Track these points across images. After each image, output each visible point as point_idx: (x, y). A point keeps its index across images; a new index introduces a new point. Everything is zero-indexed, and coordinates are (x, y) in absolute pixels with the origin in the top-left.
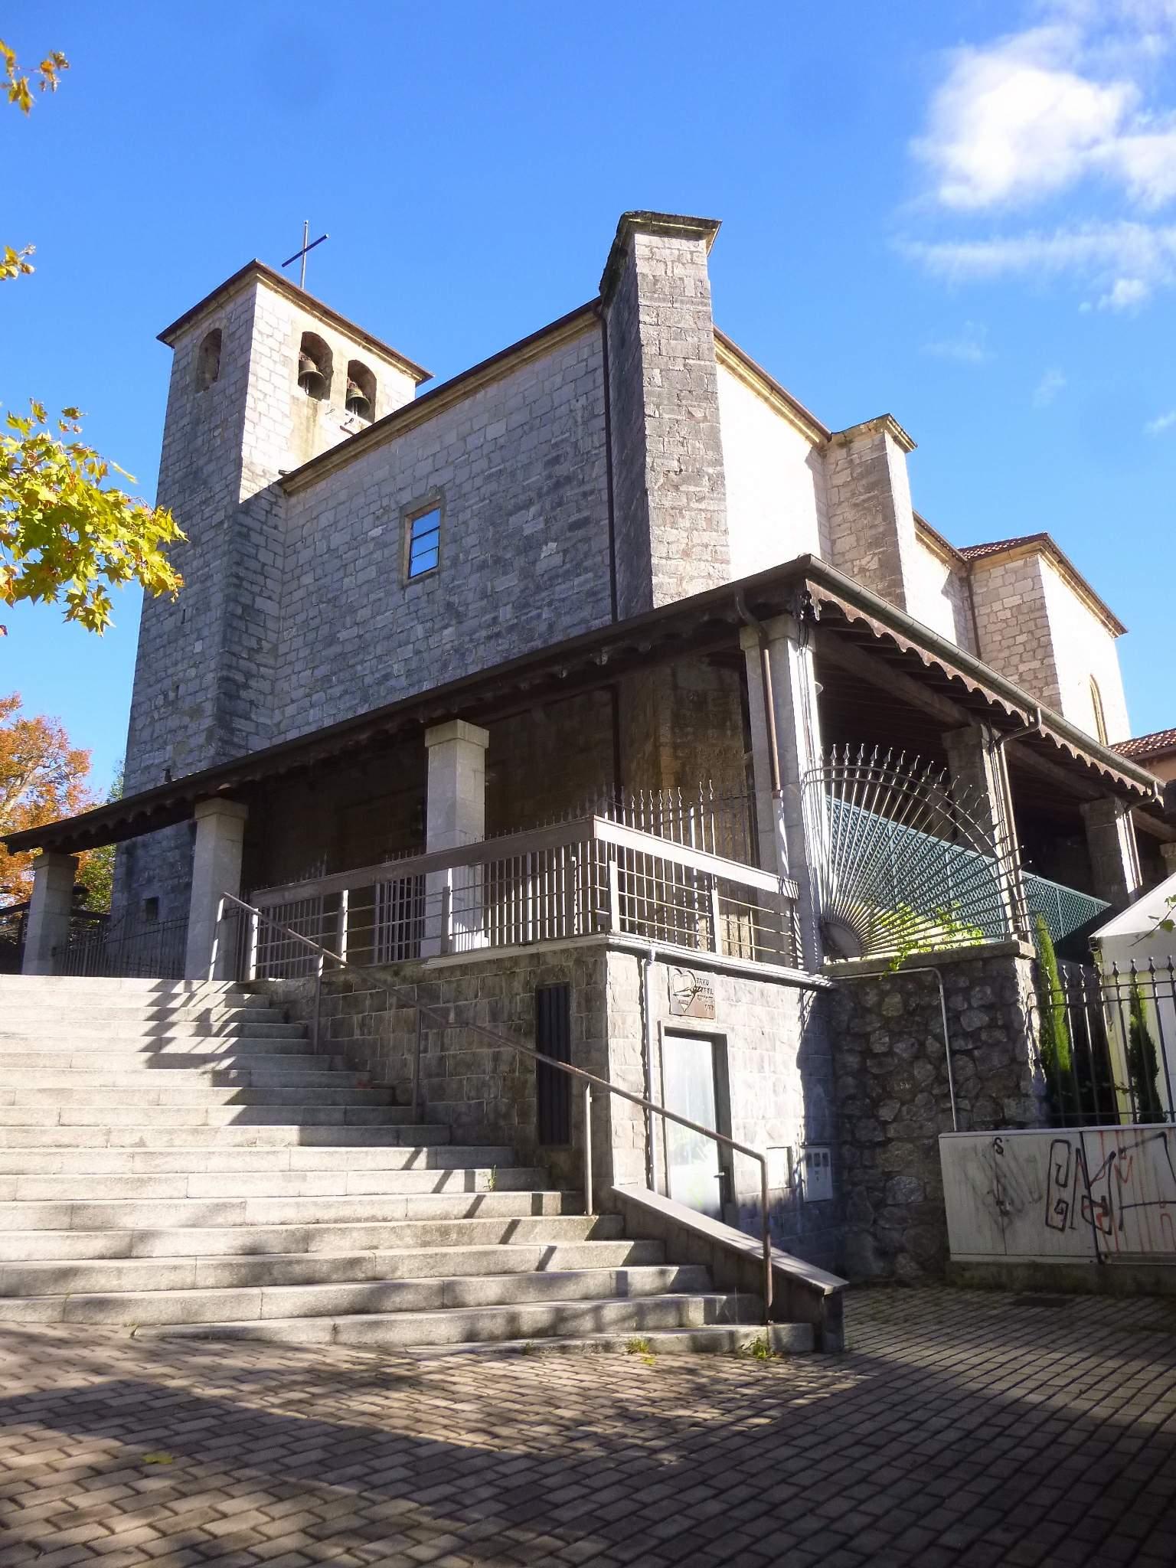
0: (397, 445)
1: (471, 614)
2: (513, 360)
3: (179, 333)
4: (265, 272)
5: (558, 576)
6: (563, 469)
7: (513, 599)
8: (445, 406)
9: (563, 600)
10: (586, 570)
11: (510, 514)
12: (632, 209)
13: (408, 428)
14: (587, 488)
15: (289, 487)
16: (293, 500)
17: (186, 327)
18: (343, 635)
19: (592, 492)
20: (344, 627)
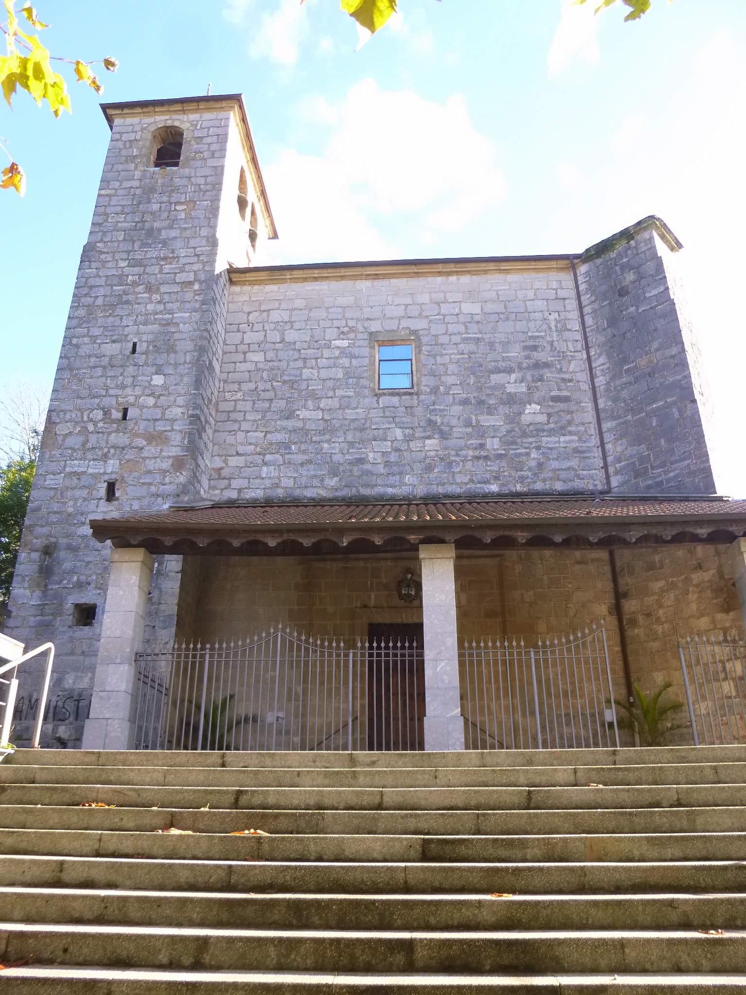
0: (363, 285)
1: (455, 435)
2: (491, 266)
3: (126, 111)
4: (241, 107)
5: (543, 431)
6: (542, 356)
7: (500, 435)
8: (417, 274)
9: (551, 449)
10: (571, 433)
11: (493, 372)
12: (658, 216)
13: (376, 277)
14: (567, 376)
15: (235, 277)
16: (237, 289)
17: (138, 110)
18: (303, 414)
19: (571, 381)
20: (304, 406)
